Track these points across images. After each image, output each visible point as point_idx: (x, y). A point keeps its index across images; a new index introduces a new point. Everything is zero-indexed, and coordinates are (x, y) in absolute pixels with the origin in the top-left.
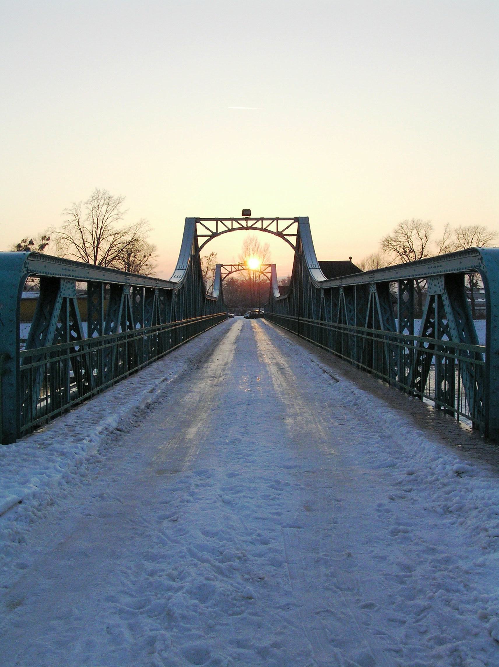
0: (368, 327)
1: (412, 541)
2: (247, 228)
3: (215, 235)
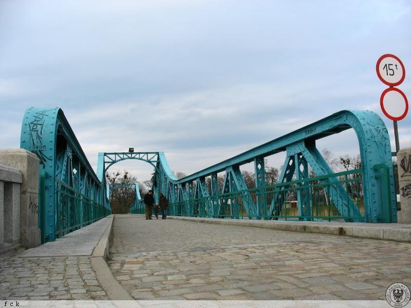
3: (114, 162)
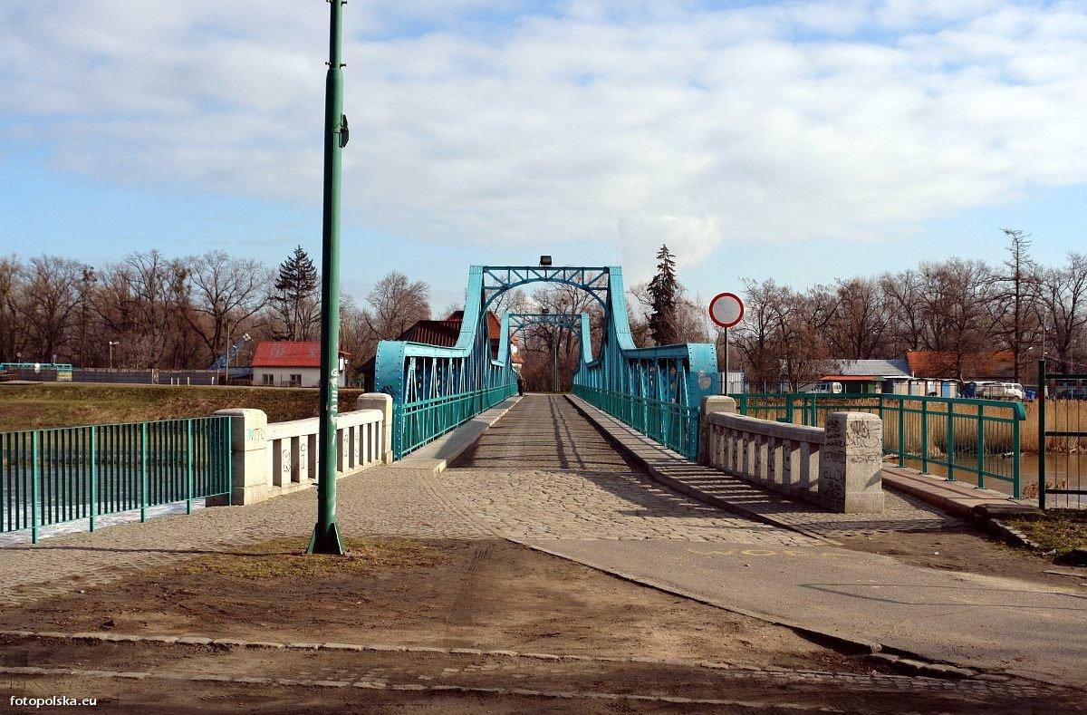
0: (455, 393)
1: (75, 312)
2: (546, 280)
